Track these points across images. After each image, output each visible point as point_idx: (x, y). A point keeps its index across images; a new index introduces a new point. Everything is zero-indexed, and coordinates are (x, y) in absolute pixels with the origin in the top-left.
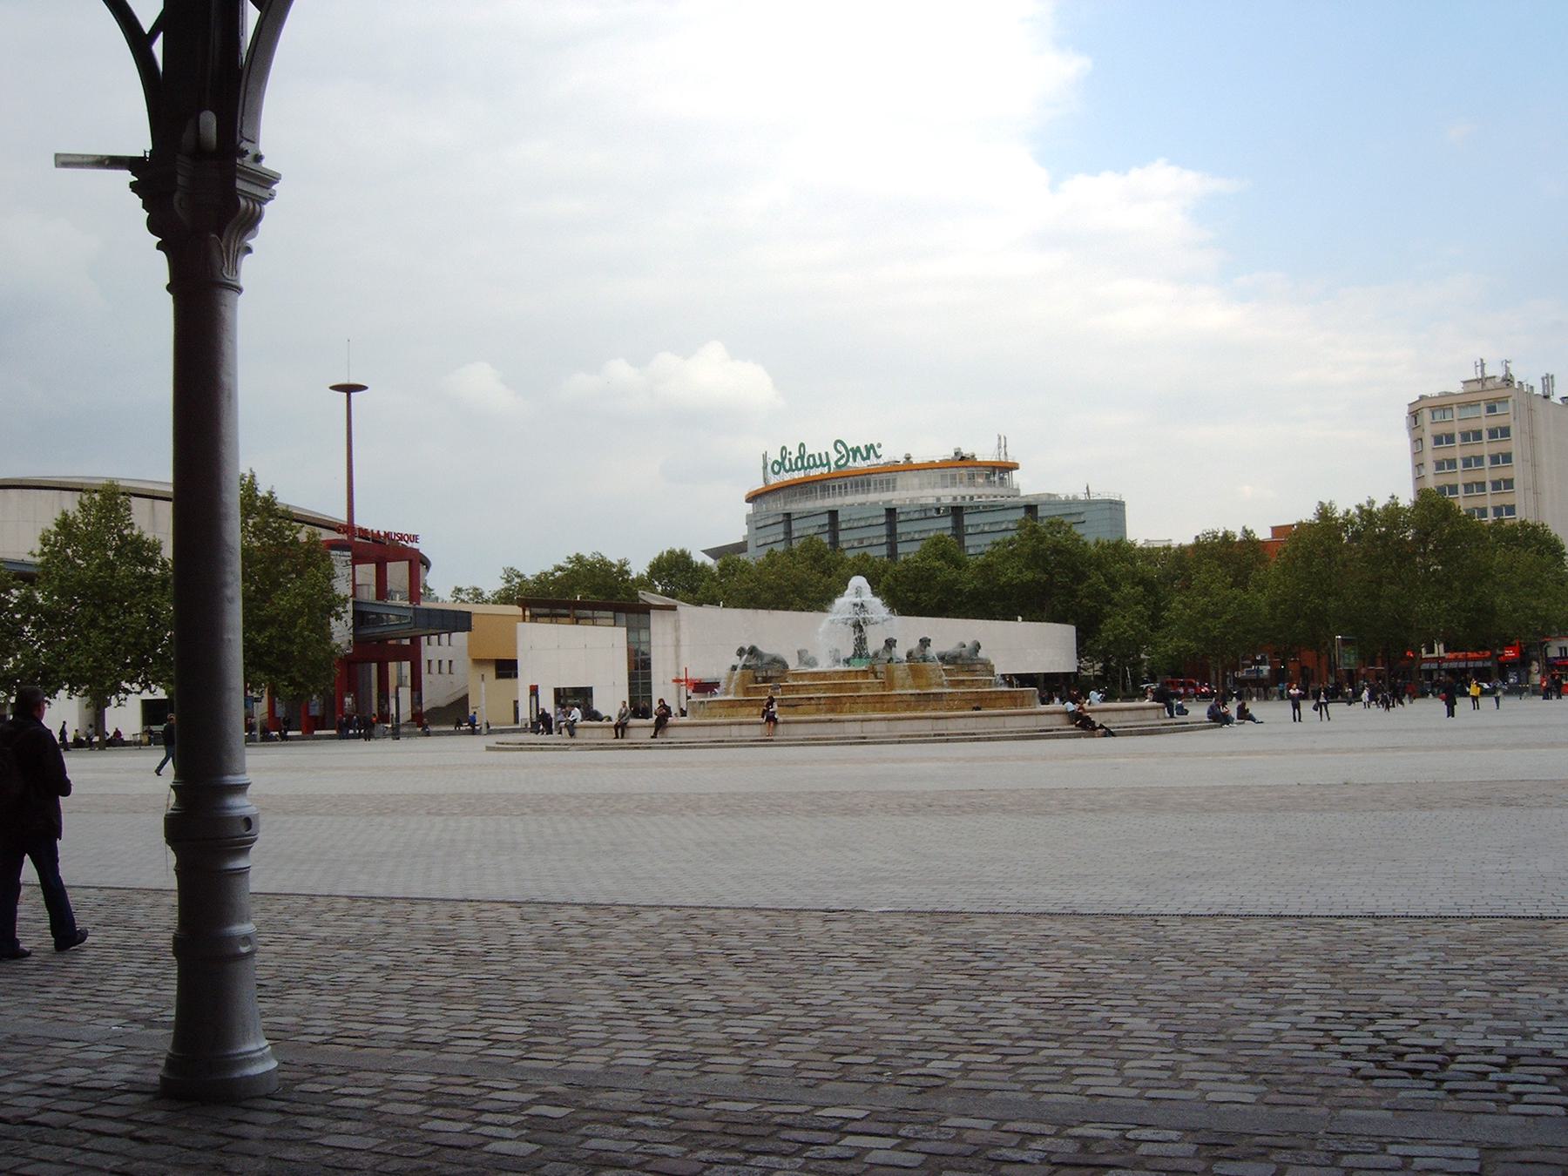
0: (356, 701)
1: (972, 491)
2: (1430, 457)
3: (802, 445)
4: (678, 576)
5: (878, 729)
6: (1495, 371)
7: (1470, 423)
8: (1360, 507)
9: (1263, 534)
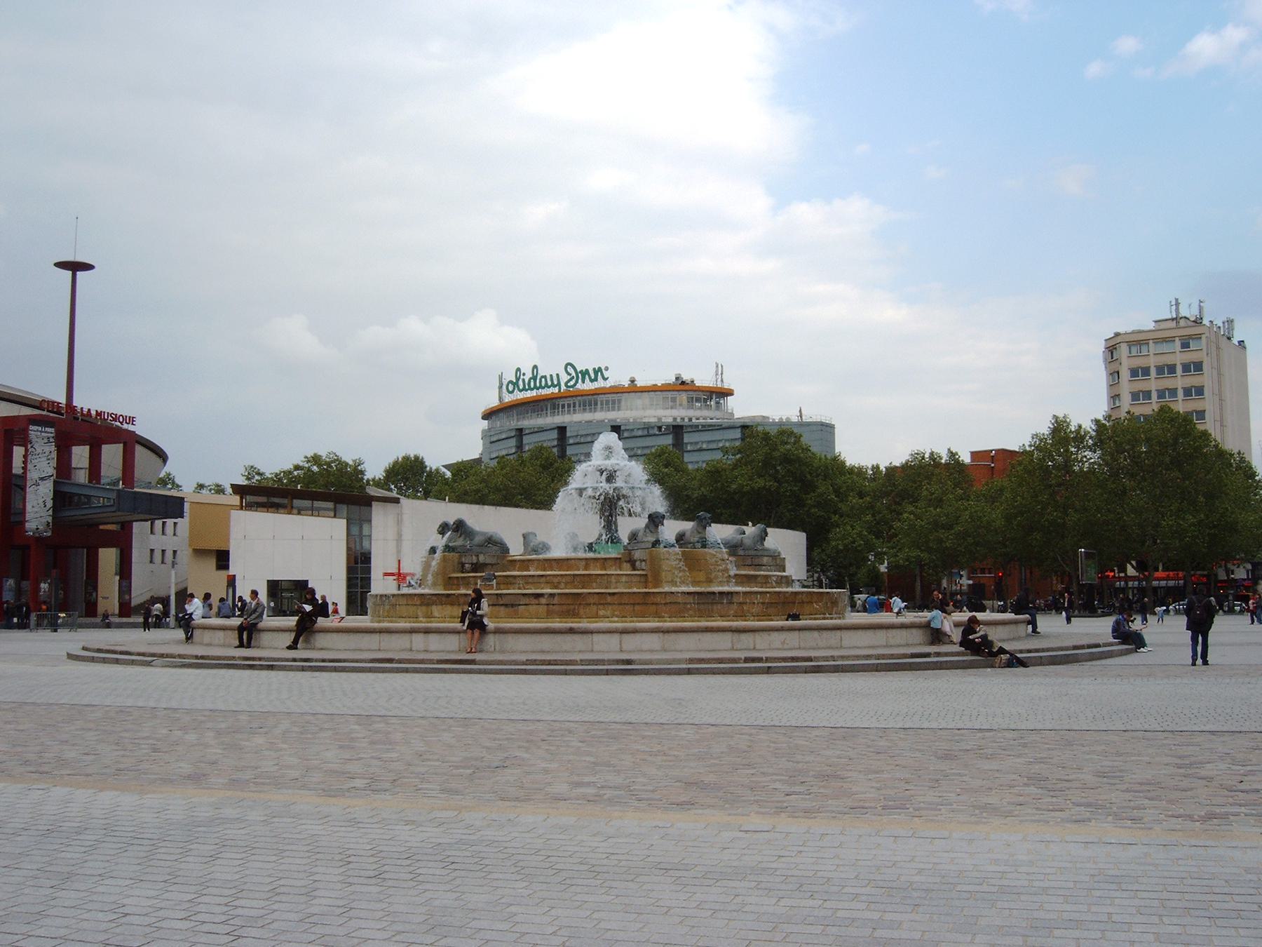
1: (691, 413)
2: (1126, 388)
3: (535, 367)
4: (410, 477)
5: (644, 646)
6: (1188, 311)
7: (1168, 359)
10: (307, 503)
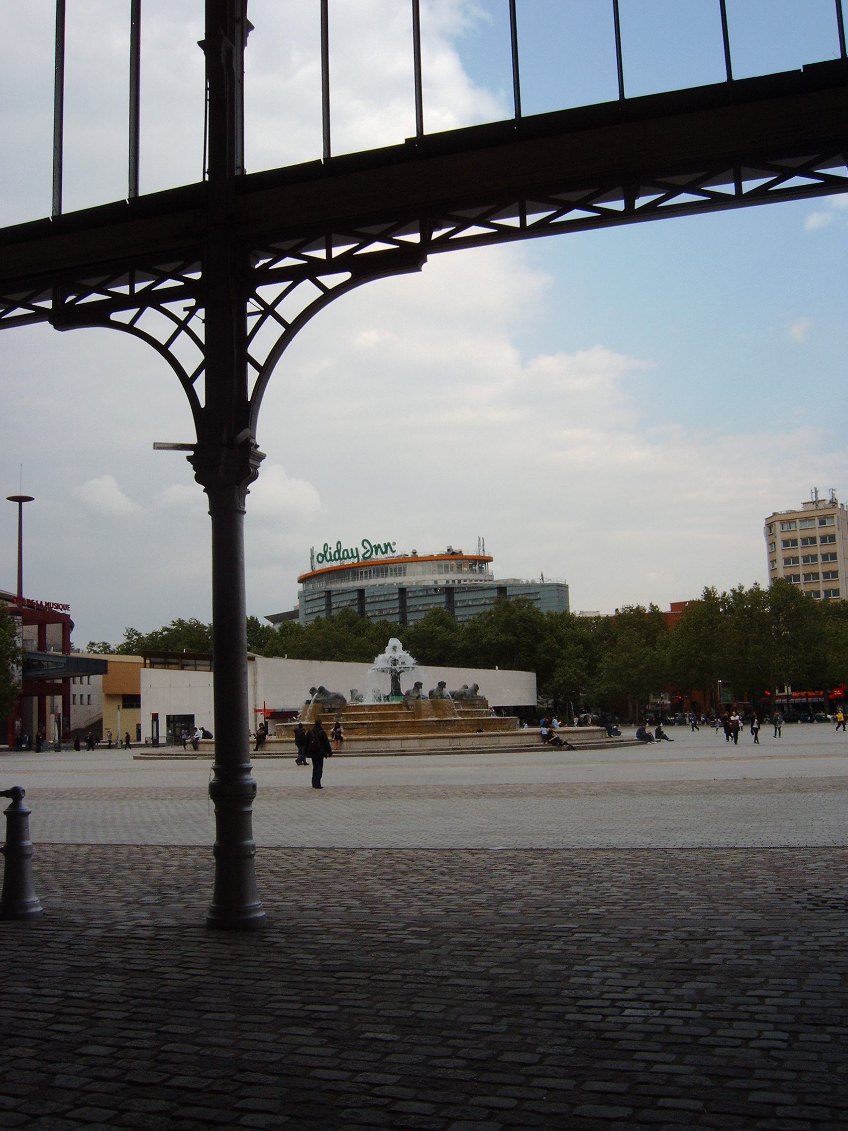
0: (22, 723)
1: (459, 576)
2: (780, 555)
3: (339, 542)
5: (413, 745)
7: (803, 533)
8: (733, 591)
9: (665, 608)
10: (192, 662)
